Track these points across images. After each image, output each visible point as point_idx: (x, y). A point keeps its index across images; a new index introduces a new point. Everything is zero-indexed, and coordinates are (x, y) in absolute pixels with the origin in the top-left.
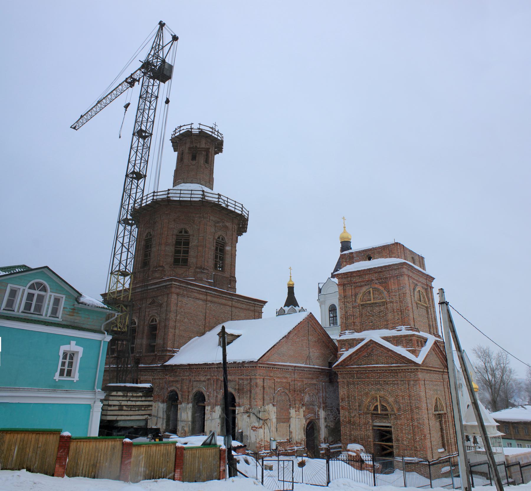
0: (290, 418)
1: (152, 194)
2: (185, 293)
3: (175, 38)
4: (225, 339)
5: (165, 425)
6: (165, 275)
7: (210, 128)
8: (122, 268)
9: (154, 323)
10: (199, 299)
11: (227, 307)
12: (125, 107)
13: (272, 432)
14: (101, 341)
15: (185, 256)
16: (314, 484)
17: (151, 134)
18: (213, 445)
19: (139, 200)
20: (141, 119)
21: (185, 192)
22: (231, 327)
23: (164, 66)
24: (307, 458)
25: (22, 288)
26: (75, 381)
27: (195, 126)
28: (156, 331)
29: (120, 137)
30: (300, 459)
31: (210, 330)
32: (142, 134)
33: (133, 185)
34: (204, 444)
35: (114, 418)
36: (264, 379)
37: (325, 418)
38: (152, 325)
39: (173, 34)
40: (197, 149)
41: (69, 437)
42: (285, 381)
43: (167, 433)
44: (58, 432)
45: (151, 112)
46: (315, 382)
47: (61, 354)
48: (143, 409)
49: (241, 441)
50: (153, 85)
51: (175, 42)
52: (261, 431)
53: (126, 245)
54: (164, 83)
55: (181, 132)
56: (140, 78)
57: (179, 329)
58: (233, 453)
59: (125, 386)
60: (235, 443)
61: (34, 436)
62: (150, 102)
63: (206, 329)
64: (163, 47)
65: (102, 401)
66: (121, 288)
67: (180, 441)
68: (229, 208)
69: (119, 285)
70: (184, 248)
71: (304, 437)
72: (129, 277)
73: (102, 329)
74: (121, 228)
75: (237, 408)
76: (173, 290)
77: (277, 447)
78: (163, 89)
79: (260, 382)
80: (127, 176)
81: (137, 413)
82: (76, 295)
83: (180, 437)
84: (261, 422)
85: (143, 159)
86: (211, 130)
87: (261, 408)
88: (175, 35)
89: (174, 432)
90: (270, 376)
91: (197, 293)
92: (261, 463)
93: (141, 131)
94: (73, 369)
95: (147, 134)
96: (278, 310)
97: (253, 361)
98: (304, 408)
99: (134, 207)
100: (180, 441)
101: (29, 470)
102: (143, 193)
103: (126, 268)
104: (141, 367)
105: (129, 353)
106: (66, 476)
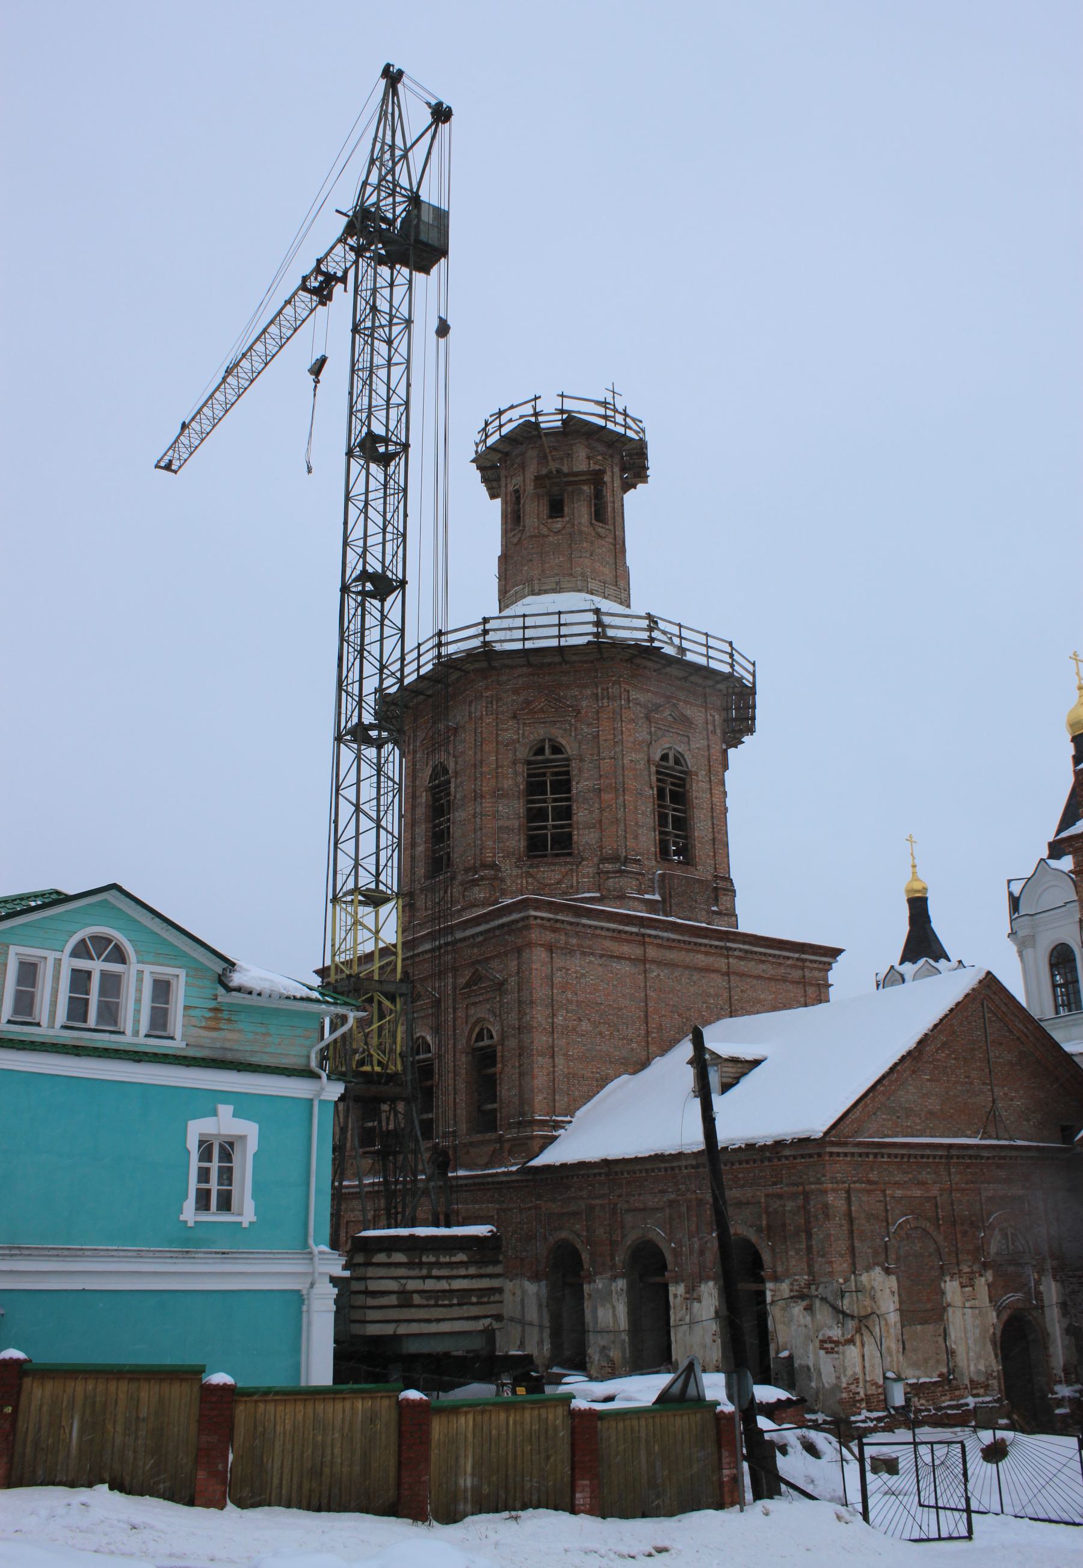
0: (944, 1309)
1: (436, 640)
2: (574, 941)
3: (441, 114)
4: (713, 1076)
5: (547, 1346)
6: (503, 893)
7: (598, 403)
8: (366, 880)
9: (486, 1042)
10: (619, 958)
11: (714, 976)
12: (311, 371)
13: (890, 1353)
14: (311, 1100)
15: (562, 827)
16: (1042, 1516)
17: (406, 446)
18: (691, 1400)
19: (398, 665)
20: (366, 400)
21: (540, 620)
22: (725, 1039)
23: (419, 216)
24: (1008, 1435)
25: (51, 956)
26: (245, 1225)
27: (549, 405)
28: (494, 1065)
29: (310, 471)
30: (987, 1437)
31: (664, 1050)
32: (375, 450)
33: (368, 617)
34: (663, 1398)
35: (388, 1329)
36: (848, 1192)
37: (1063, 1305)
38: (482, 1048)
39: (433, 102)
40: (564, 480)
41: (225, 1388)
42: (918, 1193)
43: (556, 1370)
44: (197, 1372)
45: (397, 371)
46: (1021, 1192)
47: (193, 1145)
48: (474, 1299)
49: (790, 1386)
50: (392, 285)
51: (444, 128)
52: (852, 1353)
53: (369, 808)
54: (427, 272)
55: (505, 431)
56: (346, 272)
57: (566, 1055)
58: (763, 1423)
59: (412, 1236)
60: (766, 1393)
61: (124, 1386)
62: (389, 342)
63: (653, 1048)
64: (406, 151)
65: (334, 1280)
66: (369, 947)
67: (584, 1392)
68: (690, 657)
69: (363, 934)
70: (555, 800)
71: (997, 1367)
72: (392, 903)
73: (313, 1064)
74: (347, 755)
75: (769, 1285)
76: (534, 935)
77: (908, 1400)
78: (424, 293)
79: (836, 1201)
80: (345, 589)
81: (456, 1312)
82: (218, 967)
83: (592, 1379)
84: (851, 1324)
85: (390, 528)
86: (601, 411)
87: (847, 1280)
88: (440, 104)
89: (580, 1365)
90: (870, 1182)
91: (613, 939)
92: (856, 1450)
93: (372, 439)
94: (235, 1188)
95: (391, 448)
96: (881, 977)
97: (808, 1139)
98: (989, 1275)
99: (380, 690)
100: (584, 1392)
101: (117, 1485)
102: (402, 637)
103: (378, 882)
104: (457, 1178)
105: (417, 1141)
106: (230, 1506)
